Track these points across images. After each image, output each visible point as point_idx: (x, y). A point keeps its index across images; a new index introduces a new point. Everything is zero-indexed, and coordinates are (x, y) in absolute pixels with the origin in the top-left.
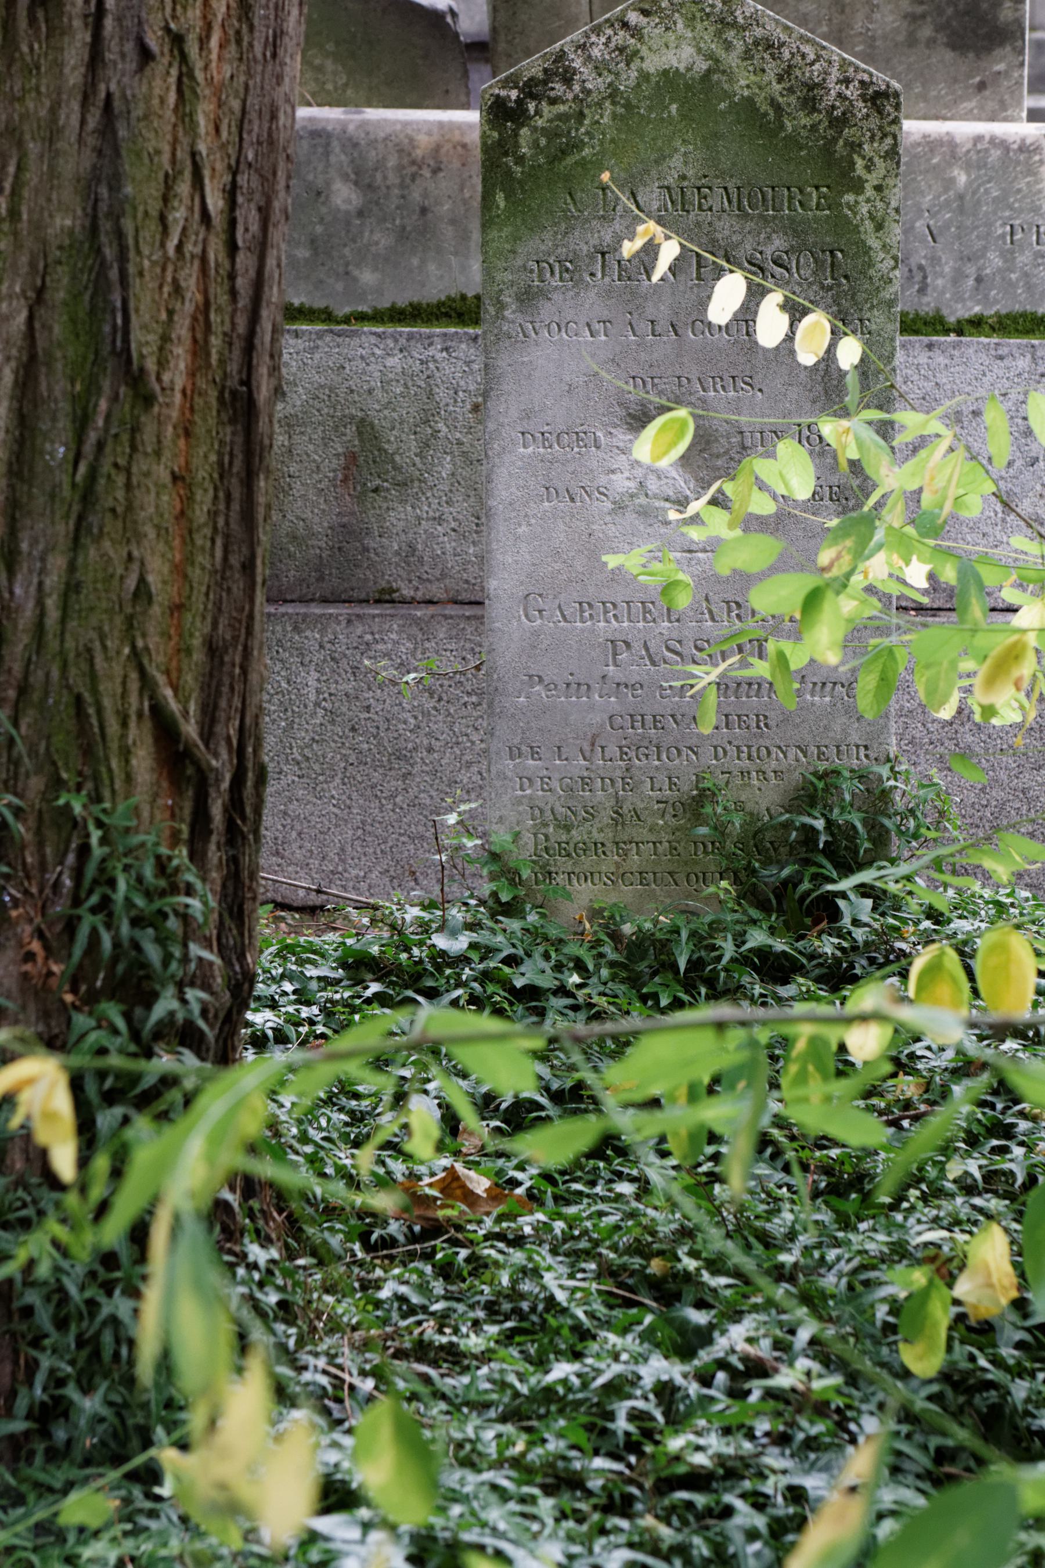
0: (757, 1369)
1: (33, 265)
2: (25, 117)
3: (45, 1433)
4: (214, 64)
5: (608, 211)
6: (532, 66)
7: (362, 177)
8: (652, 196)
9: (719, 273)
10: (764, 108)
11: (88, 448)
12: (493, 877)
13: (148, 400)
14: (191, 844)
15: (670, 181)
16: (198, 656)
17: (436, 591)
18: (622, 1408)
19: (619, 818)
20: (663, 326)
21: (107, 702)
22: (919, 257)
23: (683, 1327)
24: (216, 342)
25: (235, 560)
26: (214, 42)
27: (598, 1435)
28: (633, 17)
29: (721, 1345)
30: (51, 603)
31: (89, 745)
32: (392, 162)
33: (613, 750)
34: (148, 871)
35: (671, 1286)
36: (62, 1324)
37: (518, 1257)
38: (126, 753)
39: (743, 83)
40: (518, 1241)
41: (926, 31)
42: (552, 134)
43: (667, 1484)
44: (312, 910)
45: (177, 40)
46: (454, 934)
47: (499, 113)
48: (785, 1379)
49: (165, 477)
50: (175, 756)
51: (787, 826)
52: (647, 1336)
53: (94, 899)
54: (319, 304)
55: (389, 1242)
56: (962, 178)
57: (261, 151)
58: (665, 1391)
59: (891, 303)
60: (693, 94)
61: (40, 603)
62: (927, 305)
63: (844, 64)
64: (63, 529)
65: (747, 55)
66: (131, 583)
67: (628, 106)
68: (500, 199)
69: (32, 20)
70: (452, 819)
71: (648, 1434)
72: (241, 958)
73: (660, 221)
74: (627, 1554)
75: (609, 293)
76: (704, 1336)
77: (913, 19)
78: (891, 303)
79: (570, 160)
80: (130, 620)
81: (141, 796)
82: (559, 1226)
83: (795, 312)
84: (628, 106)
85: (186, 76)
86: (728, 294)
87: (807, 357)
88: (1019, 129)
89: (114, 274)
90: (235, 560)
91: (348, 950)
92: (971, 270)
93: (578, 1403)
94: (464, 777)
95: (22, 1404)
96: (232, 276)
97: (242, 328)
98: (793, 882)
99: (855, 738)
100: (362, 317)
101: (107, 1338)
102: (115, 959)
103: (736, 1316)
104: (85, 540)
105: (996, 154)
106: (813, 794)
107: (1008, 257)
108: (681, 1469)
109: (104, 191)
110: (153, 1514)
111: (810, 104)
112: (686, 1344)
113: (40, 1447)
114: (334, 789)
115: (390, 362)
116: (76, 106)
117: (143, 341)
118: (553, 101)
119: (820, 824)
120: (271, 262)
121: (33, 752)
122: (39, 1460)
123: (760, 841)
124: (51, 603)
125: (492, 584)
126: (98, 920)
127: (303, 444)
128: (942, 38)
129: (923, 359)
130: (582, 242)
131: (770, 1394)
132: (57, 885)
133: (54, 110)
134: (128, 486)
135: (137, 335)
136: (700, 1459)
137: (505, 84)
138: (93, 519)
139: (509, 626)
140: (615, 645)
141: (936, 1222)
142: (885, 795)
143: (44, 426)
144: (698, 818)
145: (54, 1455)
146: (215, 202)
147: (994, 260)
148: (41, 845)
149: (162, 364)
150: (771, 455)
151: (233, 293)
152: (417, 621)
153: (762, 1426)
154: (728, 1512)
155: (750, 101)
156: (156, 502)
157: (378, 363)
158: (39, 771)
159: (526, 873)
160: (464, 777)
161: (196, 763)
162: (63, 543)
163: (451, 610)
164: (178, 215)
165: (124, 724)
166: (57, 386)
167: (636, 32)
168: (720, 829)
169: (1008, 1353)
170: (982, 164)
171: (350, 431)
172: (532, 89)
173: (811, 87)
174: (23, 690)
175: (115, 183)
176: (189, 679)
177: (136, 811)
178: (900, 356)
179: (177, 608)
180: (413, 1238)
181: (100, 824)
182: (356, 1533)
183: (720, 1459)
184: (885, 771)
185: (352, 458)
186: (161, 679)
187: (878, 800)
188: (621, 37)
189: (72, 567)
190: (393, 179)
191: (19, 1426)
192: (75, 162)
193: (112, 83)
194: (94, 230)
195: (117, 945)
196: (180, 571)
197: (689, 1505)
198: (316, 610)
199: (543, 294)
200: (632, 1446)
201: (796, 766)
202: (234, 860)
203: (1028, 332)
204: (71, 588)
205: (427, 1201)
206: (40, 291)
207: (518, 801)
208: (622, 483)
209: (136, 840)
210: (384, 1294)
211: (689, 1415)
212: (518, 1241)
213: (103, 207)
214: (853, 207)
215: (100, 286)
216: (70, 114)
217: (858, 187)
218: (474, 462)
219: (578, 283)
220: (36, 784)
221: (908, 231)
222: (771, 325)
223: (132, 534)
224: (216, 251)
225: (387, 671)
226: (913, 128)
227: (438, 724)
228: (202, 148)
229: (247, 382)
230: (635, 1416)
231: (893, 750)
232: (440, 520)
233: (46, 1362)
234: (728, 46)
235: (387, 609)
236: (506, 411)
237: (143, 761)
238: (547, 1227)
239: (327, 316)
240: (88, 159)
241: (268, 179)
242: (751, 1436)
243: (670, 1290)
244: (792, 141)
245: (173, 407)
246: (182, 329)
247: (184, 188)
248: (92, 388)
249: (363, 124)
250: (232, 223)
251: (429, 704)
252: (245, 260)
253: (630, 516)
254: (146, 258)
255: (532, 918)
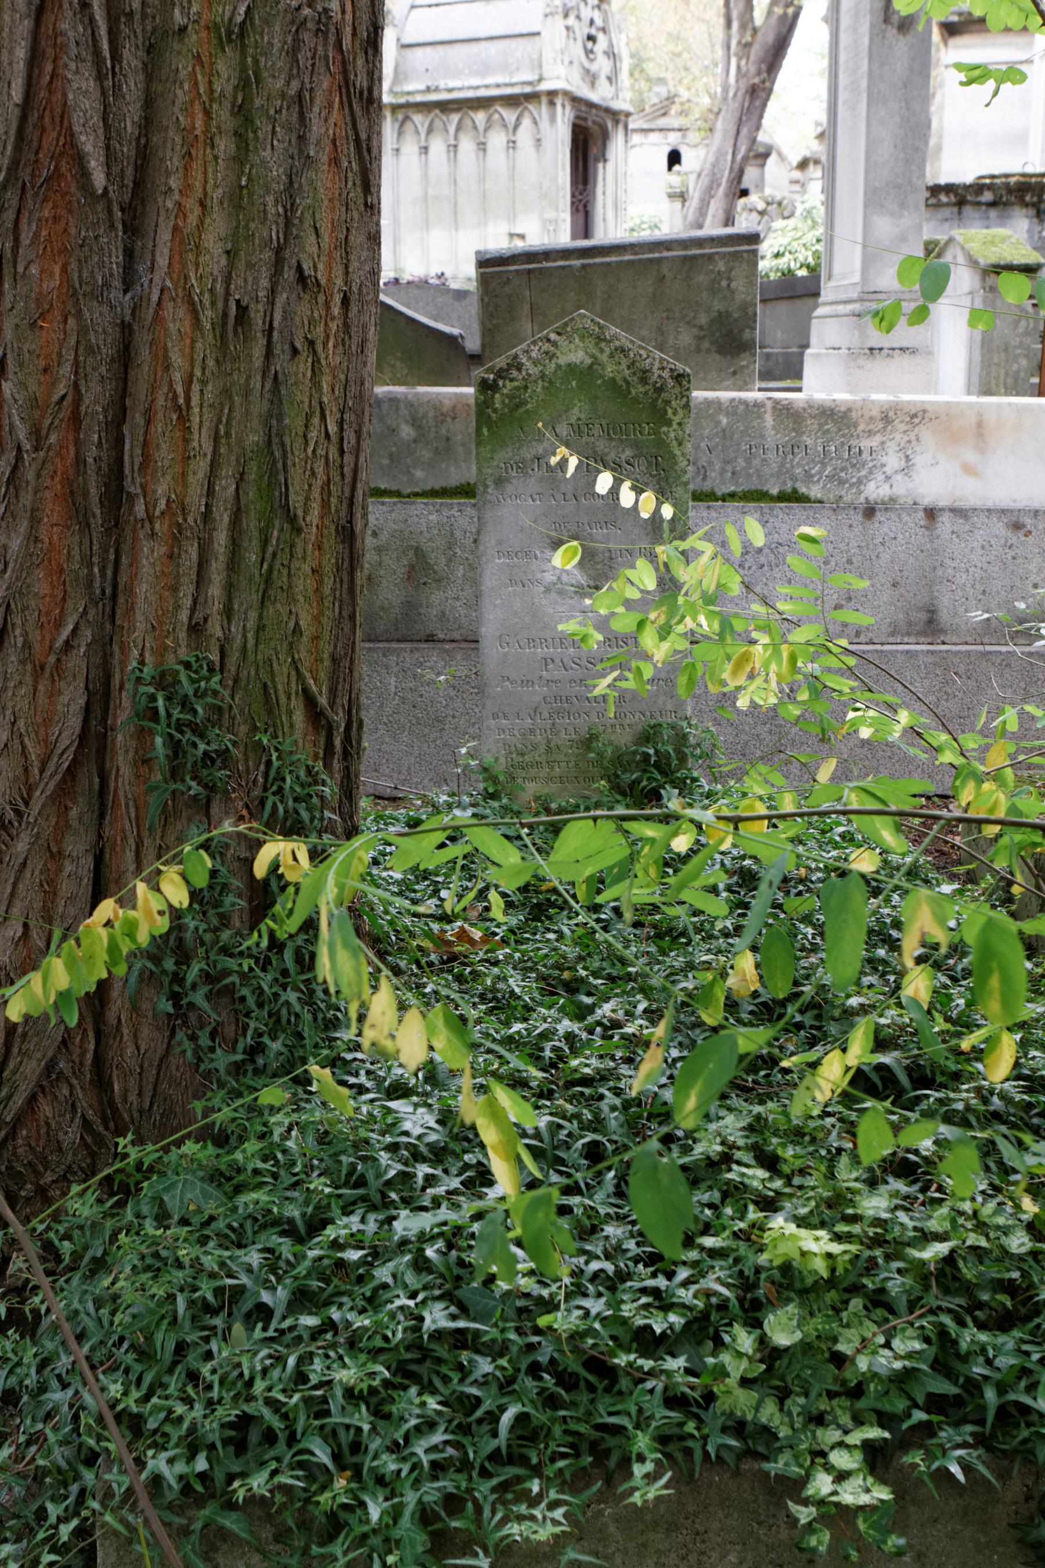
0: (616, 1025)
1: (238, 461)
2: (232, 384)
3: (253, 1061)
4: (331, 356)
5: (540, 437)
6: (501, 362)
7: (415, 422)
8: (563, 430)
9: (599, 472)
10: (621, 382)
11: (268, 556)
12: (485, 780)
13: (299, 531)
14: (324, 759)
15: (573, 421)
16: (327, 663)
17: (456, 635)
18: (548, 1046)
19: (549, 750)
20: (569, 496)
21: (280, 687)
22: (703, 462)
23: (580, 1005)
24: (334, 500)
25: (345, 614)
26: (331, 344)
27: (536, 1058)
28: (553, 336)
29: (599, 1012)
30: (250, 636)
31: (270, 707)
32: (431, 414)
33: (546, 715)
34: (302, 773)
35: (574, 985)
36: (260, 1005)
37: (496, 970)
38: (290, 713)
39: (610, 370)
40: (496, 963)
41: (706, 345)
42: (511, 397)
43: (570, 1084)
44: (394, 799)
45: (311, 343)
46: (464, 809)
47: (484, 386)
48: (629, 1029)
49: (308, 570)
50: (315, 715)
51: (635, 753)
52: (562, 1010)
53: (274, 788)
54: (394, 488)
55: (430, 964)
56: (725, 421)
57: (356, 404)
58: (570, 1037)
59: (686, 484)
60: (584, 376)
61: (244, 636)
62: (707, 486)
63: (662, 360)
64: (256, 598)
65: (611, 356)
66: (292, 625)
67: (551, 382)
68: (485, 431)
69: (235, 332)
70: (464, 751)
71: (561, 1058)
72: (351, 817)
73: (567, 446)
74: (549, 1118)
75: (541, 479)
76: (591, 1009)
77: (700, 338)
78: (686, 484)
79: (521, 410)
80: (291, 644)
81: (298, 735)
82: (517, 955)
83: (638, 491)
84: (551, 382)
85: (316, 362)
86: (604, 482)
87: (645, 515)
88: (753, 395)
89: (280, 465)
90: (345, 614)
91: (411, 818)
92: (729, 468)
93: (525, 1044)
94: (471, 731)
95: (240, 1046)
96: (342, 467)
97: (347, 494)
98: (637, 781)
99: (669, 707)
100: (416, 495)
101: (284, 1012)
102: (285, 819)
103: (607, 1000)
104: (267, 603)
105: (742, 407)
106: (648, 736)
107: (748, 461)
108: (577, 1076)
109: (274, 422)
110: (308, 1101)
111: (644, 381)
112: (581, 1013)
113: (250, 1068)
114: (405, 737)
115: (432, 517)
116: (259, 378)
117: (296, 500)
118: (512, 380)
119: (651, 751)
120: (362, 459)
121: (242, 712)
122: (250, 1074)
123: (621, 760)
124: (250, 636)
125: (483, 630)
126: (276, 799)
127: (387, 560)
128: (714, 348)
129: (705, 514)
130: (527, 453)
131: (623, 1037)
132: (255, 781)
133: (247, 381)
134: (289, 575)
135: (292, 497)
136: (587, 1070)
137: (487, 371)
138: (271, 592)
139: (491, 651)
140: (546, 661)
141: (709, 950)
142: (685, 736)
143: (245, 544)
144: (589, 749)
145: (257, 1072)
146: (332, 428)
147: (741, 463)
148: (247, 760)
149: (306, 512)
150: (633, 567)
151: (342, 475)
152: (446, 651)
153: (619, 1054)
154: (601, 1097)
155: (613, 380)
156: (303, 583)
157: (425, 517)
158: (245, 722)
159: (502, 778)
160: (471, 731)
161: (326, 718)
162: (256, 605)
163: (464, 645)
164: (313, 435)
165: (289, 698)
166: (251, 523)
167: (554, 344)
168: (601, 754)
169: (745, 1016)
170: (735, 413)
171: (411, 553)
172: (501, 374)
173: (645, 372)
174: (236, 681)
175: (280, 418)
176: (322, 675)
177: (296, 742)
178: (691, 514)
179: (316, 638)
180: (443, 962)
181: (277, 749)
182: (411, 1109)
183: (598, 1071)
184: (685, 724)
185: (412, 567)
186: (308, 675)
187: (681, 739)
188: (547, 346)
189: (261, 617)
190: (432, 423)
191: (239, 1057)
192: (259, 407)
193: (277, 366)
194: (269, 442)
195: (286, 811)
196: (317, 619)
197: (582, 1094)
198: (395, 645)
199: (508, 480)
200: (553, 1065)
201: (638, 721)
202: (347, 768)
203: (758, 500)
204: (260, 628)
205: (449, 943)
206: (242, 475)
207: (497, 741)
208: (549, 577)
209: (295, 757)
210: (428, 990)
211: (582, 1047)
212: (496, 963)
213: (274, 431)
214: (667, 434)
215: (273, 472)
216: (256, 382)
217: (669, 423)
218: (473, 568)
219: (526, 474)
220: (244, 729)
221: (697, 447)
222: (627, 497)
223: (292, 600)
224: (333, 454)
225: (429, 676)
226: (698, 395)
227: (458, 704)
228: (325, 400)
229: (350, 522)
230: (555, 1049)
231: (689, 713)
232: (457, 599)
233: (252, 1025)
234: (602, 351)
235: (431, 645)
236: (489, 540)
237: (299, 717)
238: (511, 956)
239: (398, 494)
240: (266, 405)
241: (359, 415)
242: (613, 1058)
243: (573, 987)
244: (636, 400)
245: (312, 534)
246: (316, 494)
247: (316, 420)
248: (270, 524)
249: (417, 394)
250: (342, 439)
251: (453, 693)
252: (348, 458)
253: (553, 595)
254: (297, 456)
255: (505, 801)
